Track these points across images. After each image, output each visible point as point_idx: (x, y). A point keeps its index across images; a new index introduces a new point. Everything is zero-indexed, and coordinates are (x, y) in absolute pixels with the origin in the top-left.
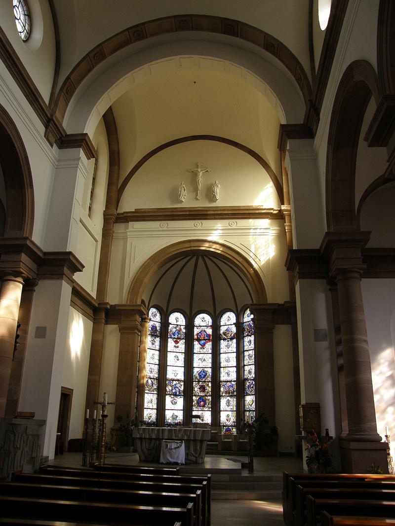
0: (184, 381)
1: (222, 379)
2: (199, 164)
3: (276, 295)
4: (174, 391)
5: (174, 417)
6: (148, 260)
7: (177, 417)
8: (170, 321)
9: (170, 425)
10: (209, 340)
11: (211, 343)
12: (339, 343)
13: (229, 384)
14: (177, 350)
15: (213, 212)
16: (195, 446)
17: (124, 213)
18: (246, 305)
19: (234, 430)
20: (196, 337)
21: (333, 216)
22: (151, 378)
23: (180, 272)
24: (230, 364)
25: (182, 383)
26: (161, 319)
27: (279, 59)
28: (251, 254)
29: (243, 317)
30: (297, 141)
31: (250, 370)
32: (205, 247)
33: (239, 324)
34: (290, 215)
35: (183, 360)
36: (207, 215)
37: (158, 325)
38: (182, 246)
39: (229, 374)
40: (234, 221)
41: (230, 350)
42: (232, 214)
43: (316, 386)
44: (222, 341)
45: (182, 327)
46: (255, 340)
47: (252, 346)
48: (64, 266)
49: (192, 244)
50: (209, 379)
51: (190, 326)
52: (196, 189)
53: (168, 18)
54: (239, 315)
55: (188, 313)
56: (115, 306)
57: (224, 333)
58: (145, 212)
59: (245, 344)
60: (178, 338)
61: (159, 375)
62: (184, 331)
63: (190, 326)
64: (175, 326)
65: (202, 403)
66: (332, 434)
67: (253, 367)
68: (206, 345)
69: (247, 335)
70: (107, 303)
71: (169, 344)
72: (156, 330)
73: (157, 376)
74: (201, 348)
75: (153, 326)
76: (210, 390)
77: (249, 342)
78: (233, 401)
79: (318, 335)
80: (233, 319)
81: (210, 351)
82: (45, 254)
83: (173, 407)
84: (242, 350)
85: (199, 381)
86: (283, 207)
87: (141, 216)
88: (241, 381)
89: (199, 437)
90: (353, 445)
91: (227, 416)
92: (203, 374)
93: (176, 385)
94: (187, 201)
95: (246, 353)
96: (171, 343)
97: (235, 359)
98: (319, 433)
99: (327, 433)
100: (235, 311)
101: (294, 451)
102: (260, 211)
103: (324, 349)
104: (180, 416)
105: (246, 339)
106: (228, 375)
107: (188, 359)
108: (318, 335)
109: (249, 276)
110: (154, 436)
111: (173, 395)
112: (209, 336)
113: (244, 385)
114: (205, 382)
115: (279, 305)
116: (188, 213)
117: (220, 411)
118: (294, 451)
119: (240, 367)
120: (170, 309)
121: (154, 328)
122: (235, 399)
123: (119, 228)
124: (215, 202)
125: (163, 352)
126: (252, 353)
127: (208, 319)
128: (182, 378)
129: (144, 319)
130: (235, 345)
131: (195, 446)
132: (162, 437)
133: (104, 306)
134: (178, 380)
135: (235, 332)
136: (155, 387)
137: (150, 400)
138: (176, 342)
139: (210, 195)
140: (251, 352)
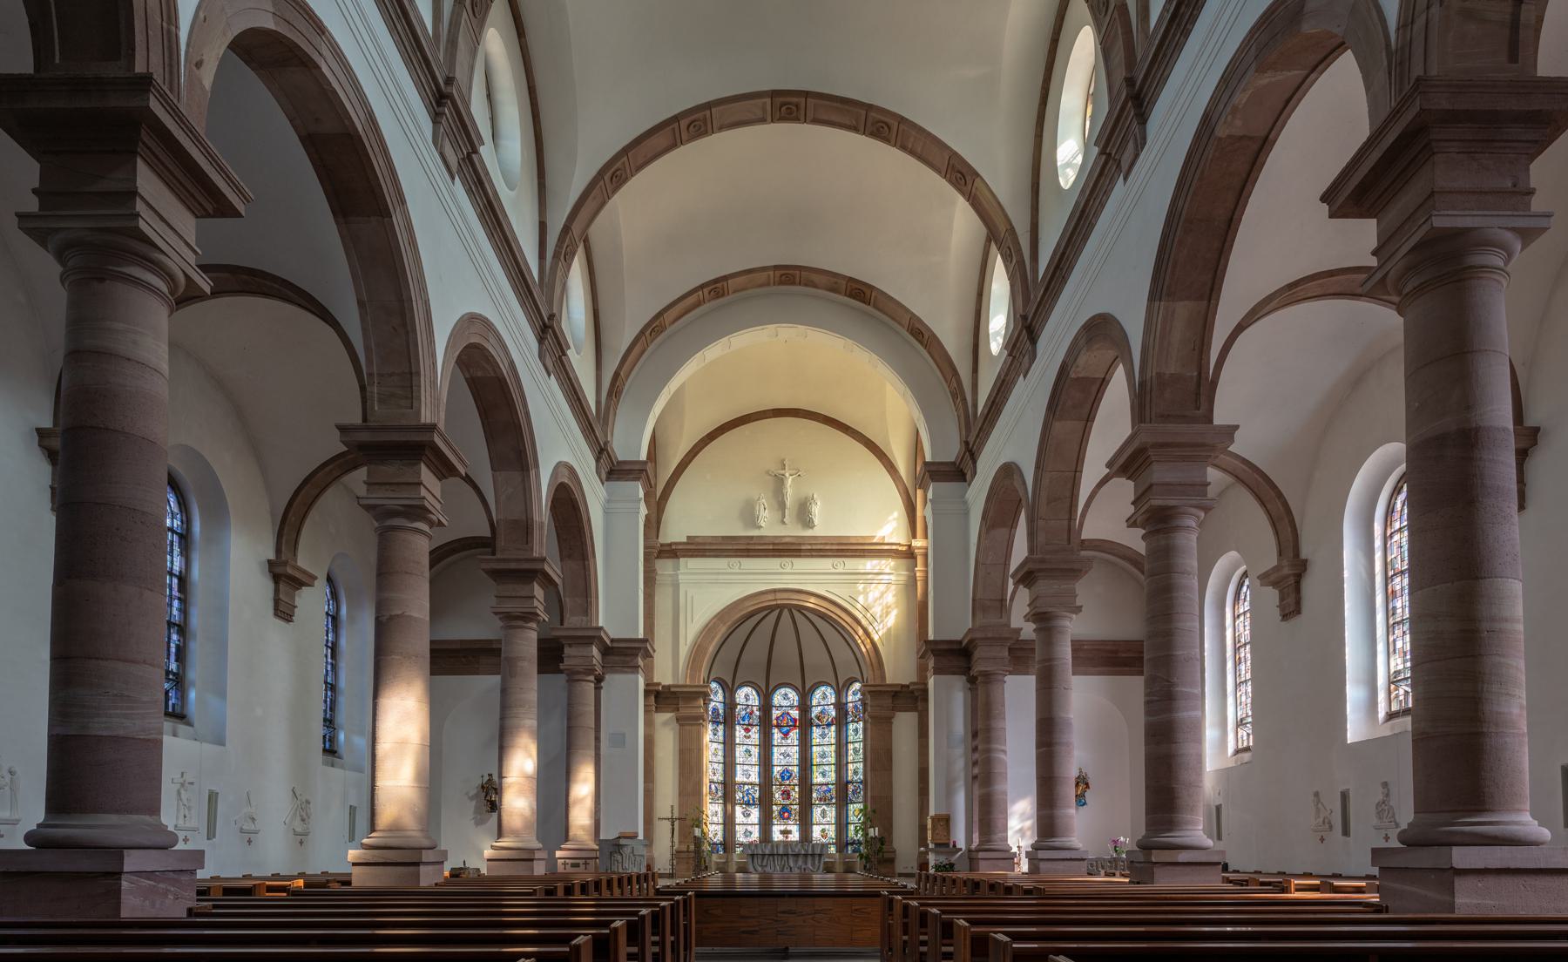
1: (815, 781)
2: (786, 463)
3: (899, 669)
4: (746, 799)
5: (747, 833)
6: (713, 618)
7: (751, 833)
8: (737, 700)
9: (741, 845)
10: (795, 726)
12: (975, 749)
14: (748, 741)
15: (809, 547)
16: (813, 860)
17: (670, 545)
18: (851, 678)
19: (832, 849)
20: (775, 722)
21: (978, 606)
22: (714, 783)
23: (754, 628)
25: (757, 788)
26: (724, 697)
27: (929, 353)
29: (847, 696)
31: (856, 768)
33: (840, 706)
34: (926, 555)
36: (800, 550)
39: (824, 776)
40: (841, 560)
42: (838, 550)
45: (755, 709)
49: (779, 596)
50: (796, 781)
51: (766, 707)
54: (840, 691)
56: (669, 686)
57: (818, 718)
58: (704, 544)
59: (849, 734)
61: (724, 778)
62: (758, 713)
63: (766, 707)
64: (744, 707)
65: (786, 814)
66: (961, 844)
67: (861, 766)
68: (791, 734)
69: (852, 721)
70: (659, 684)
71: (737, 734)
72: (718, 714)
73: (721, 778)
74: (783, 739)
75: (714, 709)
81: (796, 743)
82: (612, 641)
83: (745, 820)
84: (845, 742)
85: (781, 785)
86: (918, 543)
87: (698, 548)
88: (842, 785)
89: (818, 851)
90: (981, 855)
91: (823, 826)
92: (786, 775)
93: (748, 790)
94: (769, 525)
95: (851, 747)
96: (739, 732)
104: (756, 835)
105: (851, 727)
106: (824, 775)
110: (767, 852)
111: (746, 804)
112: (795, 720)
115: (902, 686)
116: (771, 547)
117: (812, 824)
119: (841, 765)
123: (664, 567)
125: (729, 744)
126: (859, 746)
127: (793, 696)
128: (757, 781)
129: (706, 697)
130: (833, 734)
131: (813, 860)
132: (813, 850)
133: (656, 688)
134: (751, 784)
136: (720, 794)
138: (747, 730)
140: (857, 745)
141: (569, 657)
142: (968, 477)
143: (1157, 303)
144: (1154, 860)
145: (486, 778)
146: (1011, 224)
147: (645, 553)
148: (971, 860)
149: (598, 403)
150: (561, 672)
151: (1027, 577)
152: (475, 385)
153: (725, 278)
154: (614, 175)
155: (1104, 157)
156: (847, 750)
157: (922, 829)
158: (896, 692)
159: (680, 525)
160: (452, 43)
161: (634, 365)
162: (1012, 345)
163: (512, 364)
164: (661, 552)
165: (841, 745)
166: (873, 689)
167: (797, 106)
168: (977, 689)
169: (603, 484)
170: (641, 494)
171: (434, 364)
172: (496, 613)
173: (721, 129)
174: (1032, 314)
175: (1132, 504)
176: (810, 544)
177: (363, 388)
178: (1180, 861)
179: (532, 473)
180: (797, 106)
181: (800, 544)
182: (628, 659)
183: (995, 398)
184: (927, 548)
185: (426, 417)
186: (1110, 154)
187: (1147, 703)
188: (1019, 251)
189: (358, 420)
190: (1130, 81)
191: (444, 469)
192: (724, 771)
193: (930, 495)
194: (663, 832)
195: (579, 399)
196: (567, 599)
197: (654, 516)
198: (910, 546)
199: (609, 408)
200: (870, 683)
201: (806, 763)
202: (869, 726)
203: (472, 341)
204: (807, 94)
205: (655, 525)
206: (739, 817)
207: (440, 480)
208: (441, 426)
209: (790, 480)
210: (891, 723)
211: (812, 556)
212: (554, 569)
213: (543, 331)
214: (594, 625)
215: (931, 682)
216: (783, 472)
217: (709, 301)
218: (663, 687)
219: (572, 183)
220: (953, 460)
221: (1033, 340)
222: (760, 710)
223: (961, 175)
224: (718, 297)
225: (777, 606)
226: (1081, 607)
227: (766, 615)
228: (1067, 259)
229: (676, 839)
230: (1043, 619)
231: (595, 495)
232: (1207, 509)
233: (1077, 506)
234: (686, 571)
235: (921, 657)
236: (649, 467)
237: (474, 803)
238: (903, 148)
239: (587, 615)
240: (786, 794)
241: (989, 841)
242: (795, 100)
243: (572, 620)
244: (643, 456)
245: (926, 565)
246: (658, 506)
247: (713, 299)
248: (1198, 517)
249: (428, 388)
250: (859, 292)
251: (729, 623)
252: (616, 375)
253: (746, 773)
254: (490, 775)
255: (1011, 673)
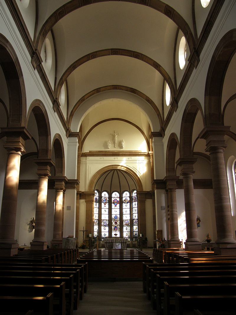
0: (108, 220)
1: (124, 219)
3: (147, 187)
4: (104, 224)
5: (105, 235)
8: (102, 196)
9: (103, 238)
10: (118, 203)
11: (119, 204)
12: (168, 211)
13: (127, 221)
15: (122, 154)
20: (113, 202)
21: (168, 170)
24: (127, 213)
25: (108, 221)
26: (99, 195)
27: (151, 105)
28: (137, 171)
30: (157, 138)
31: (135, 216)
32: (119, 168)
33: (131, 197)
34: (153, 155)
35: (108, 211)
36: (119, 154)
37: (98, 198)
38: (109, 167)
41: (127, 207)
43: (161, 224)
44: (123, 204)
45: (107, 198)
46: (137, 204)
47: (136, 206)
48: (75, 184)
49: (114, 167)
50: (119, 219)
52: (114, 143)
53: (110, 86)
54: (131, 193)
55: (109, 192)
56: (84, 192)
57: (125, 200)
59: (133, 205)
60: (106, 203)
62: (108, 199)
63: (110, 197)
66: (166, 239)
67: (137, 214)
70: (81, 191)
72: (97, 200)
73: (98, 218)
75: (96, 198)
76: (119, 223)
77: (135, 204)
78: (129, 228)
79: (162, 208)
80: (128, 195)
82: (68, 180)
85: (114, 220)
86: (150, 152)
87: (92, 154)
88: (132, 220)
90: (172, 242)
91: (126, 234)
92: (116, 217)
94: (111, 148)
96: (103, 204)
97: (129, 211)
98: (162, 239)
99: (164, 239)
100: (129, 191)
101: (153, 246)
102: (141, 153)
103: (164, 213)
104: (107, 235)
105: (134, 203)
107: (110, 211)
108: (162, 208)
109: (136, 180)
112: (118, 201)
113: (133, 222)
114: (117, 220)
115: (148, 192)
116: (111, 154)
118: (153, 246)
119: (131, 214)
120: (102, 191)
121: (96, 199)
122: (129, 227)
123: (83, 159)
124: (122, 148)
125: (100, 208)
126: (136, 209)
129: (93, 195)
132: (123, 241)
133: (80, 193)
134: (106, 220)
135: (129, 200)
136: (97, 223)
137: (96, 228)
138: (105, 204)
139: (120, 146)
141: (57, 185)
142: (163, 136)
143: (207, 96)
144: (220, 247)
145: (32, 219)
146: (169, 77)
147: (78, 155)
148: (169, 243)
149: (67, 118)
150: (54, 189)
151: (180, 163)
152: (36, 115)
153: (100, 88)
154: (74, 67)
155: (190, 64)
156: (133, 210)
157: (155, 233)
158: (146, 193)
159: (86, 149)
160: (38, 42)
161: (76, 109)
162: (172, 104)
163: (46, 110)
164: (82, 155)
165: (131, 209)
166: (140, 193)
167: (117, 52)
168: (168, 193)
169: (67, 138)
170: (77, 141)
171: (26, 112)
172: (37, 174)
173: (99, 57)
174: (176, 97)
175: (206, 145)
176: (122, 153)
177: (8, 118)
178: (228, 247)
179: (49, 137)
180: (117, 52)
181: (119, 153)
182: (72, 185)
183: (168, 117)
184: (153, 154)
185: (23, 125)
186: (192, 63)
187: (215, 200)
188: (172, 83)
189: (6, 126)
190: (194, 48)
191: (26, 138)
192: (98, 216)
193: (153, 140)
194: (81, 234)
195: (62, 117)
196: (57, 169)
197: (80, 146)
198: (148, 153)
199: (70, 119)
200: (139, 191)
201: (121, 214)
202: (139, 203)
203: (36, 106)
204: (119, 49)
205: (81, 148)
206: (103, 230)
207: (25, 140)
208: (26, 127)
209: (116, 136)
210: (145, 202)
211: (122, 156)
212: (53, 162)
213: (54, 102)
214: (63, 176)
215: (155, 191)
216: (114, 134)
217: (96, 93)
218: (82, 192)
219: (63, 70)
220: (159, 131)
221: (177, 103)
222: (108, 198)
223: (157, 66)
224: (98, 92)
225: (113, 169)
226: (195, 171)
227: (110, 172)
228: (184, 85)
229: (84, 237)
230: (186, 174)
231: (65, 141)
232: (225, 147)
233: (192, 145)
234: (89, 160)
235: (153, 184)
236: (80, 134)
237: (29, 226)
238: (143, 60)
239: (62, 173)
240: (116, 223)
241: (173, 238)
242: (117, 51)
243: (58, 175)
244: (78, 131)
245: (153, 158)
246: (81, 143)
247: (97, 93)
248: (223, 149)
249: (24, 118)
250: (133, 91)
251: (100, 174)
252: (72, 111)
253: (105, 216)
254: (33, 218)
255: (177, 189)
